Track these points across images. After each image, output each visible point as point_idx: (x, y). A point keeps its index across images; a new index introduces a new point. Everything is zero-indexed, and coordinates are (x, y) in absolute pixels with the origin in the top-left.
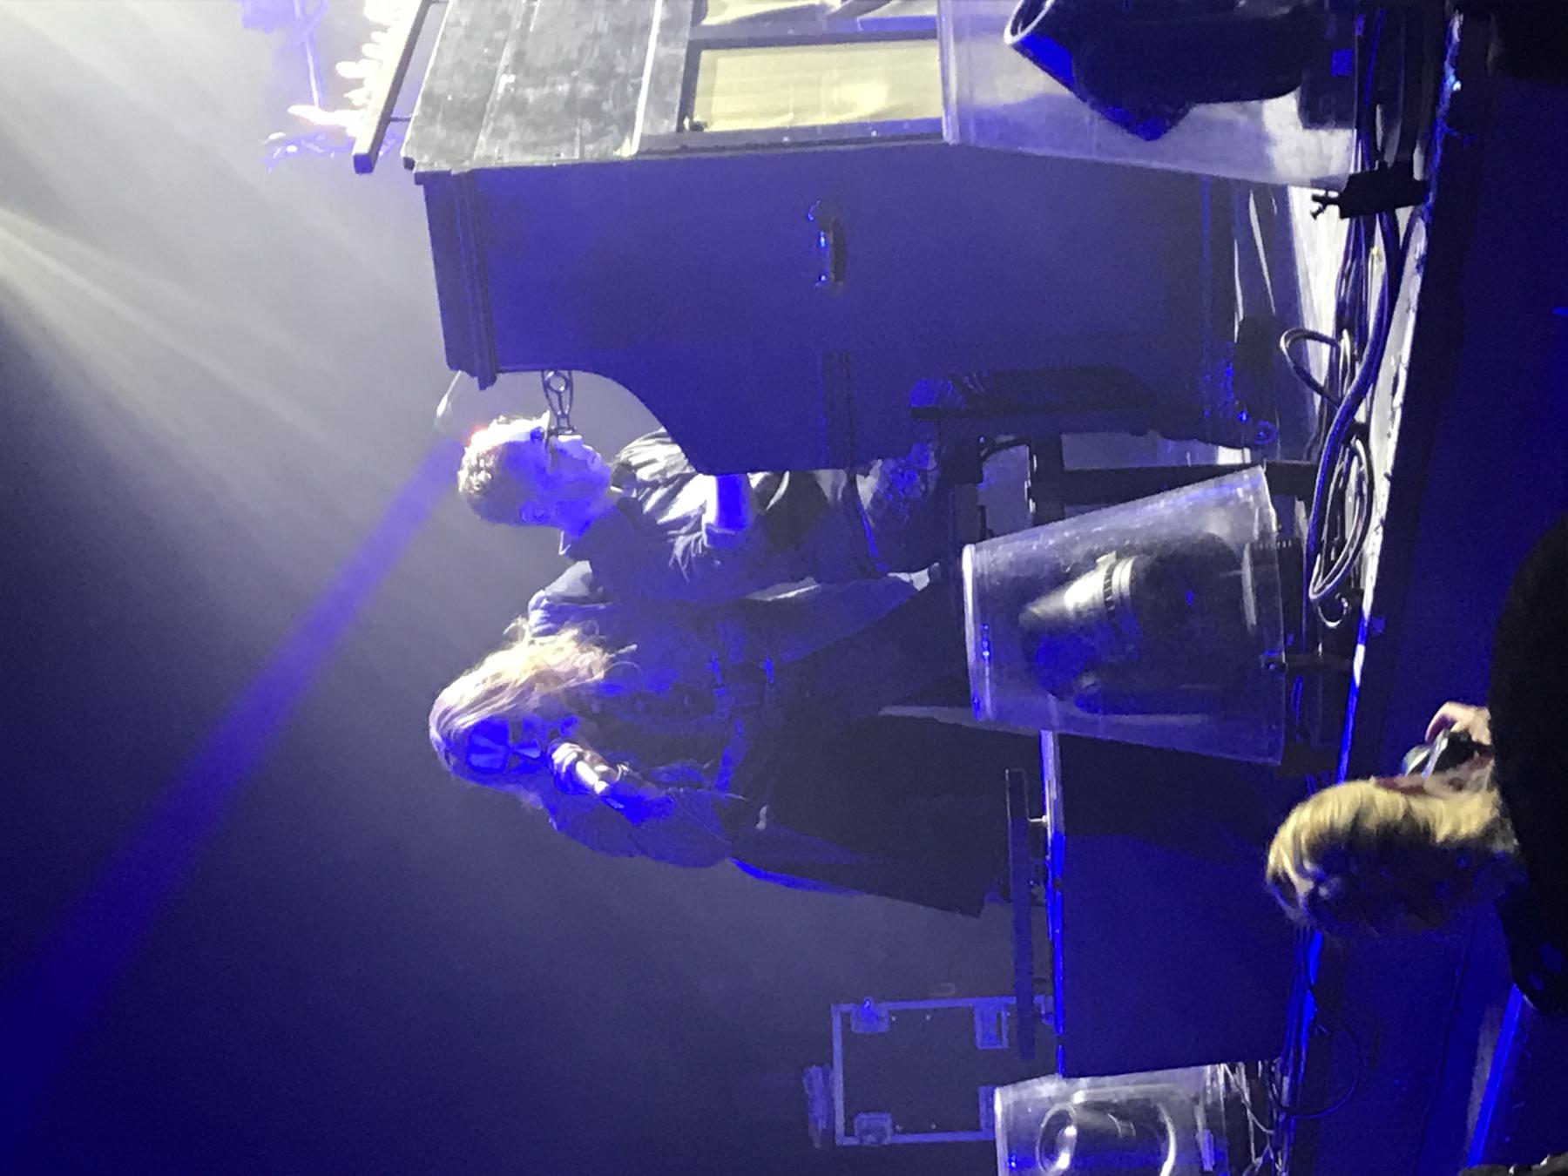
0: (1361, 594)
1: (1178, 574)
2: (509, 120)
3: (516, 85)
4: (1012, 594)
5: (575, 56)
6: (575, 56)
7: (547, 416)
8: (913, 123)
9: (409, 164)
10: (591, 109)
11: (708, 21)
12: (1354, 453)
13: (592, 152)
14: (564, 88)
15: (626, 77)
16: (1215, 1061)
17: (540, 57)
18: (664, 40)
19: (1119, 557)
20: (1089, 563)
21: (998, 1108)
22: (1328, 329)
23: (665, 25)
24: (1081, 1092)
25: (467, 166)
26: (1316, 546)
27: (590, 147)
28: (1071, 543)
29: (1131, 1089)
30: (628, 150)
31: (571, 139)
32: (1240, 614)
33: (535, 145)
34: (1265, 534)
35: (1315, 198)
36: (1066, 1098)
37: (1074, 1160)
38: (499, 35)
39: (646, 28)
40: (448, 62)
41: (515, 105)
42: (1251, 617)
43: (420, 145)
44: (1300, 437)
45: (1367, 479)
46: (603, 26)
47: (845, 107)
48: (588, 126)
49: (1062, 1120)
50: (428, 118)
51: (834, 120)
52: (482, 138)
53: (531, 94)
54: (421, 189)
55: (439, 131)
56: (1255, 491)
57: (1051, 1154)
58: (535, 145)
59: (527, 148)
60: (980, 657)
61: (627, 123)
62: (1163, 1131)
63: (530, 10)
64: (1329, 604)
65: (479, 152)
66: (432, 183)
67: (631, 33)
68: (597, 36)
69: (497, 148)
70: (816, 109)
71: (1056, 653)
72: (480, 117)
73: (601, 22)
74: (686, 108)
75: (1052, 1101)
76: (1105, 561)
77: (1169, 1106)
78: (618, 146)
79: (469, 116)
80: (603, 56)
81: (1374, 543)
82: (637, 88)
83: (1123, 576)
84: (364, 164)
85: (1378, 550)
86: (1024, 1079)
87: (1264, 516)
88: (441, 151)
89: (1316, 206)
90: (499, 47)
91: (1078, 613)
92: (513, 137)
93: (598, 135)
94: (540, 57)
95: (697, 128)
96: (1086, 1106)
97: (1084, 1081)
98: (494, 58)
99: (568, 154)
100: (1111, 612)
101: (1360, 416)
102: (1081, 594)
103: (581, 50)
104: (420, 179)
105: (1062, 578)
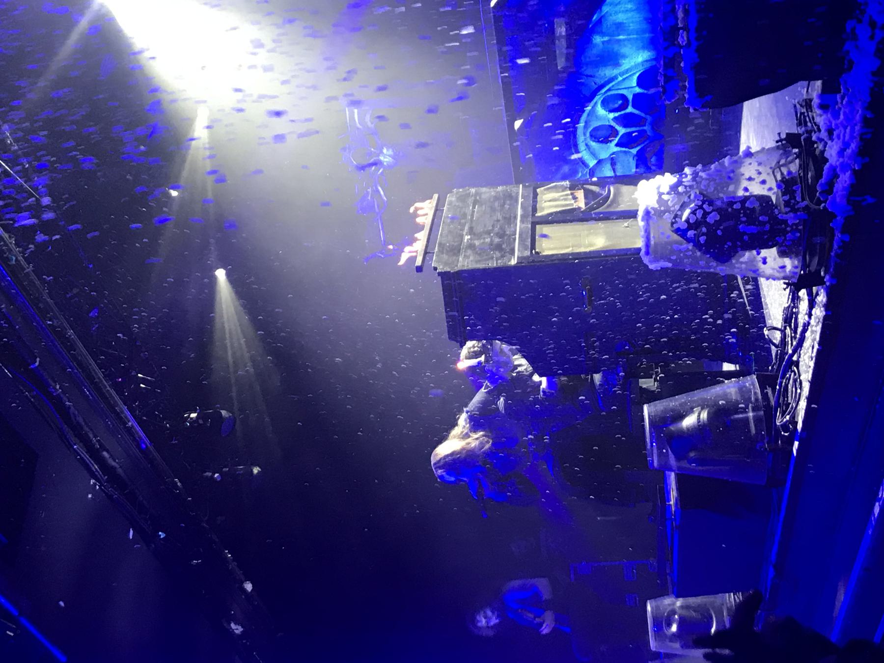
0: (797, 423)
1: (722, 414)
2: (469, 252)
3: (471, 239)
4: (662, 423)
5: (490, 228)
6: (490, 228)
7: (483, 356)
8: (617, 250)
9: (435, 269)
10: (498, 247)
11: (539, 214)
12: (792, 371)
13: (500, 263)
14: (488, 240)
15: (510, 236)
16: (729, 592)
17: (479, 229)
18: (522, 221)
19: (702, 409)
20: (690, 411)
21: (649, 608)
22: (779, 324)
23: (522, 216)
24: (679, 603)
25: (456, 269)
26: (778, 405)
27: (499, 261)
28: (685, 403)
29: (705, 600)
30: (513, 262)
31: (492, 258)
32: (749, 431)
33: (480, 261)
34: (757, 400)
35: (785, 283)
36: (674, 604)
37: (679, 627)
38: (463, 221)
39: (515, 218)
40: (446, 232)
41: (471, 246)
42: (753, 431)
43: (438, 261)
44: (773, 368)
45: (798, 383)
46: (500, 217)
47: (591, 245)
48: (498, 254)
49: (674, 612)
50: (441, 251)
51: (588, 250)
52: (461, 259)
53: (477, 243)
54: (439, 278)
55: (445, 257)
56: (753, 384)
57: (669, 625)
58: (480, 261)
59: (477, 262)
60: (652, 446)
61: (512, 252)
62: (711, 618)
63: (473, 212)
64: (785, 427)
65: (460, 264)
66: (444, 275)
67: (510, 219)
68: (498, 221)
69: (466, 262)
70: (580, 247)
71: (683, 443)
72: (459, 251)
73: (499, 216)
74: (533, 246)
75: (669, 605)
76: (697, 410)
77: (713, 608)
78: (510, 260)
79: (455, 251)
80: (501, 228)
81: (803, 404)
82: (515, 239)
83: (704, 415)
84: (419, 269)
85: (804, 407)
86: (660, 596)
87: (755, 393)
88: (446, 264)
89: (785, 286)
90: (464, 225)
91: (688, 429)
92: (471, 258)
93: (503, 256)
94: (479, 229)
95: (537, 253)
96: (682, 607)
97: (681, 599)
98: (462, 230)
99: (493, 264)
100: (701, 429)
101: (795, 358)
102: (689, 421)
103: (493, 226)
104: (440, 274)
105: (682, 417)
